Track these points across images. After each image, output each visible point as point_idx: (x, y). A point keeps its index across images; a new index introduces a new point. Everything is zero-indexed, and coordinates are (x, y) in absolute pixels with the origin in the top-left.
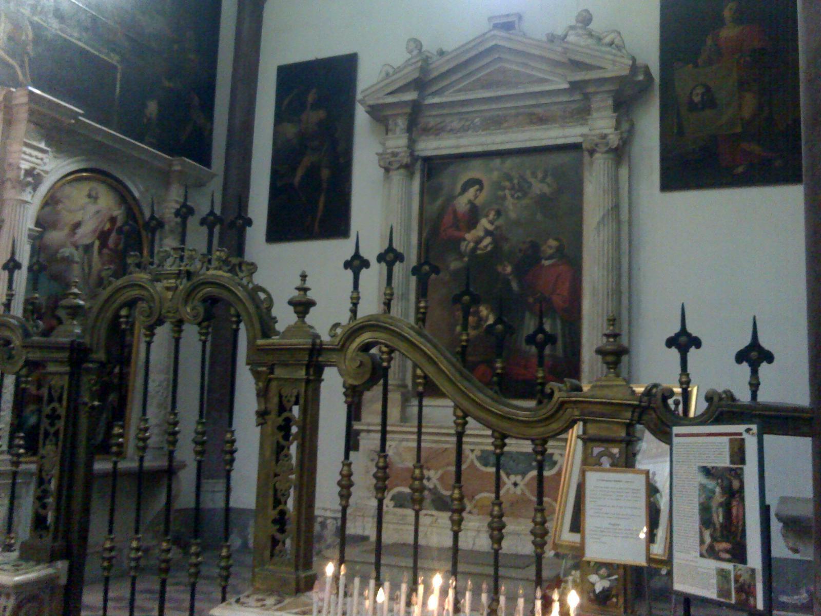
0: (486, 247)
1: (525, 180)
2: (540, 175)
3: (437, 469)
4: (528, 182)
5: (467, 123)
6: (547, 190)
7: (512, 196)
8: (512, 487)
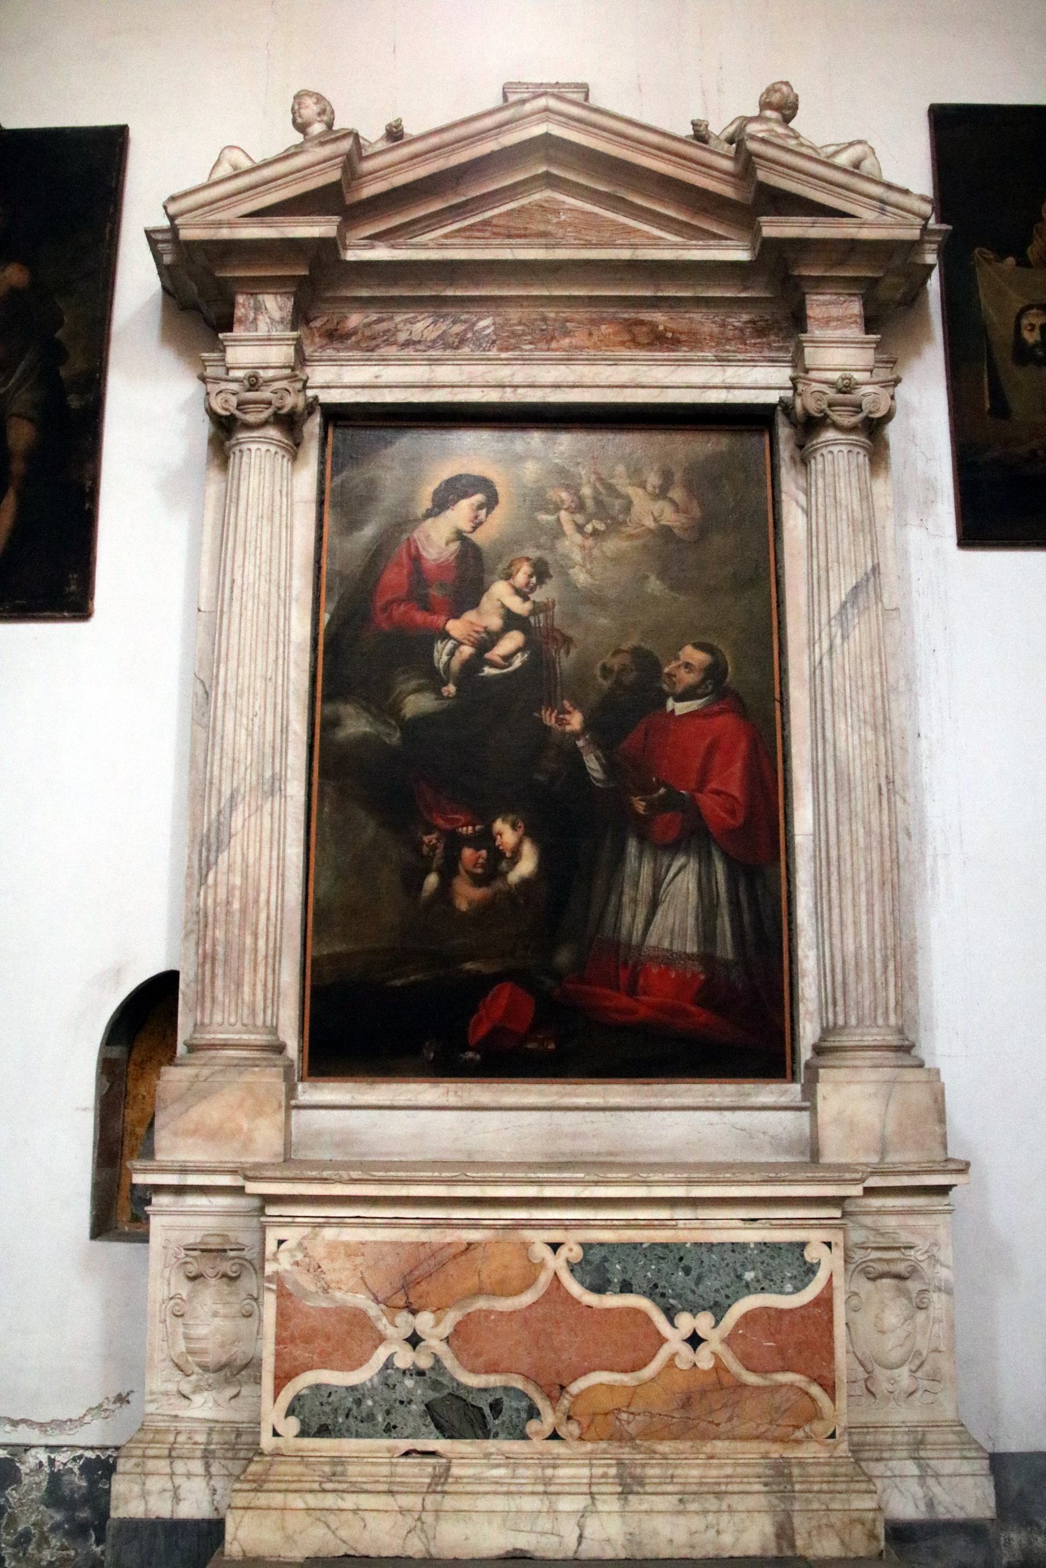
0: (508, 658)
1: (611, 488)
2: (653, 480)
3: (439, 1310)
4: (619, 496)
5: (458, 328)
6: (670, 517)
7: (580, 528)
8: (686, 1349)
